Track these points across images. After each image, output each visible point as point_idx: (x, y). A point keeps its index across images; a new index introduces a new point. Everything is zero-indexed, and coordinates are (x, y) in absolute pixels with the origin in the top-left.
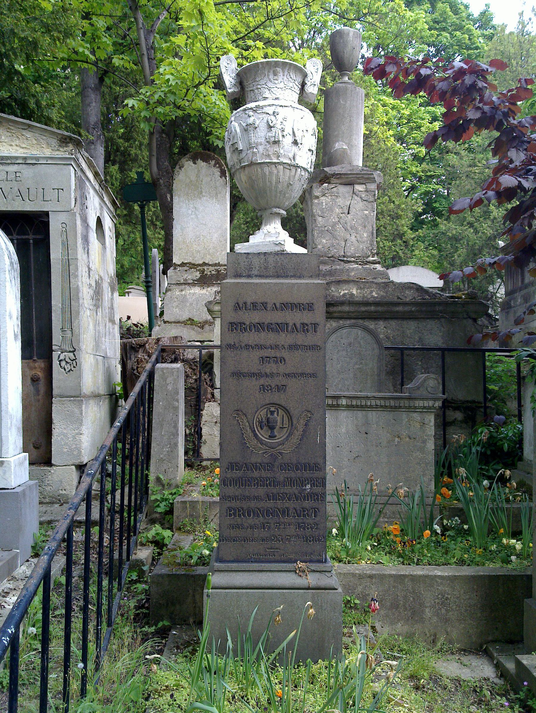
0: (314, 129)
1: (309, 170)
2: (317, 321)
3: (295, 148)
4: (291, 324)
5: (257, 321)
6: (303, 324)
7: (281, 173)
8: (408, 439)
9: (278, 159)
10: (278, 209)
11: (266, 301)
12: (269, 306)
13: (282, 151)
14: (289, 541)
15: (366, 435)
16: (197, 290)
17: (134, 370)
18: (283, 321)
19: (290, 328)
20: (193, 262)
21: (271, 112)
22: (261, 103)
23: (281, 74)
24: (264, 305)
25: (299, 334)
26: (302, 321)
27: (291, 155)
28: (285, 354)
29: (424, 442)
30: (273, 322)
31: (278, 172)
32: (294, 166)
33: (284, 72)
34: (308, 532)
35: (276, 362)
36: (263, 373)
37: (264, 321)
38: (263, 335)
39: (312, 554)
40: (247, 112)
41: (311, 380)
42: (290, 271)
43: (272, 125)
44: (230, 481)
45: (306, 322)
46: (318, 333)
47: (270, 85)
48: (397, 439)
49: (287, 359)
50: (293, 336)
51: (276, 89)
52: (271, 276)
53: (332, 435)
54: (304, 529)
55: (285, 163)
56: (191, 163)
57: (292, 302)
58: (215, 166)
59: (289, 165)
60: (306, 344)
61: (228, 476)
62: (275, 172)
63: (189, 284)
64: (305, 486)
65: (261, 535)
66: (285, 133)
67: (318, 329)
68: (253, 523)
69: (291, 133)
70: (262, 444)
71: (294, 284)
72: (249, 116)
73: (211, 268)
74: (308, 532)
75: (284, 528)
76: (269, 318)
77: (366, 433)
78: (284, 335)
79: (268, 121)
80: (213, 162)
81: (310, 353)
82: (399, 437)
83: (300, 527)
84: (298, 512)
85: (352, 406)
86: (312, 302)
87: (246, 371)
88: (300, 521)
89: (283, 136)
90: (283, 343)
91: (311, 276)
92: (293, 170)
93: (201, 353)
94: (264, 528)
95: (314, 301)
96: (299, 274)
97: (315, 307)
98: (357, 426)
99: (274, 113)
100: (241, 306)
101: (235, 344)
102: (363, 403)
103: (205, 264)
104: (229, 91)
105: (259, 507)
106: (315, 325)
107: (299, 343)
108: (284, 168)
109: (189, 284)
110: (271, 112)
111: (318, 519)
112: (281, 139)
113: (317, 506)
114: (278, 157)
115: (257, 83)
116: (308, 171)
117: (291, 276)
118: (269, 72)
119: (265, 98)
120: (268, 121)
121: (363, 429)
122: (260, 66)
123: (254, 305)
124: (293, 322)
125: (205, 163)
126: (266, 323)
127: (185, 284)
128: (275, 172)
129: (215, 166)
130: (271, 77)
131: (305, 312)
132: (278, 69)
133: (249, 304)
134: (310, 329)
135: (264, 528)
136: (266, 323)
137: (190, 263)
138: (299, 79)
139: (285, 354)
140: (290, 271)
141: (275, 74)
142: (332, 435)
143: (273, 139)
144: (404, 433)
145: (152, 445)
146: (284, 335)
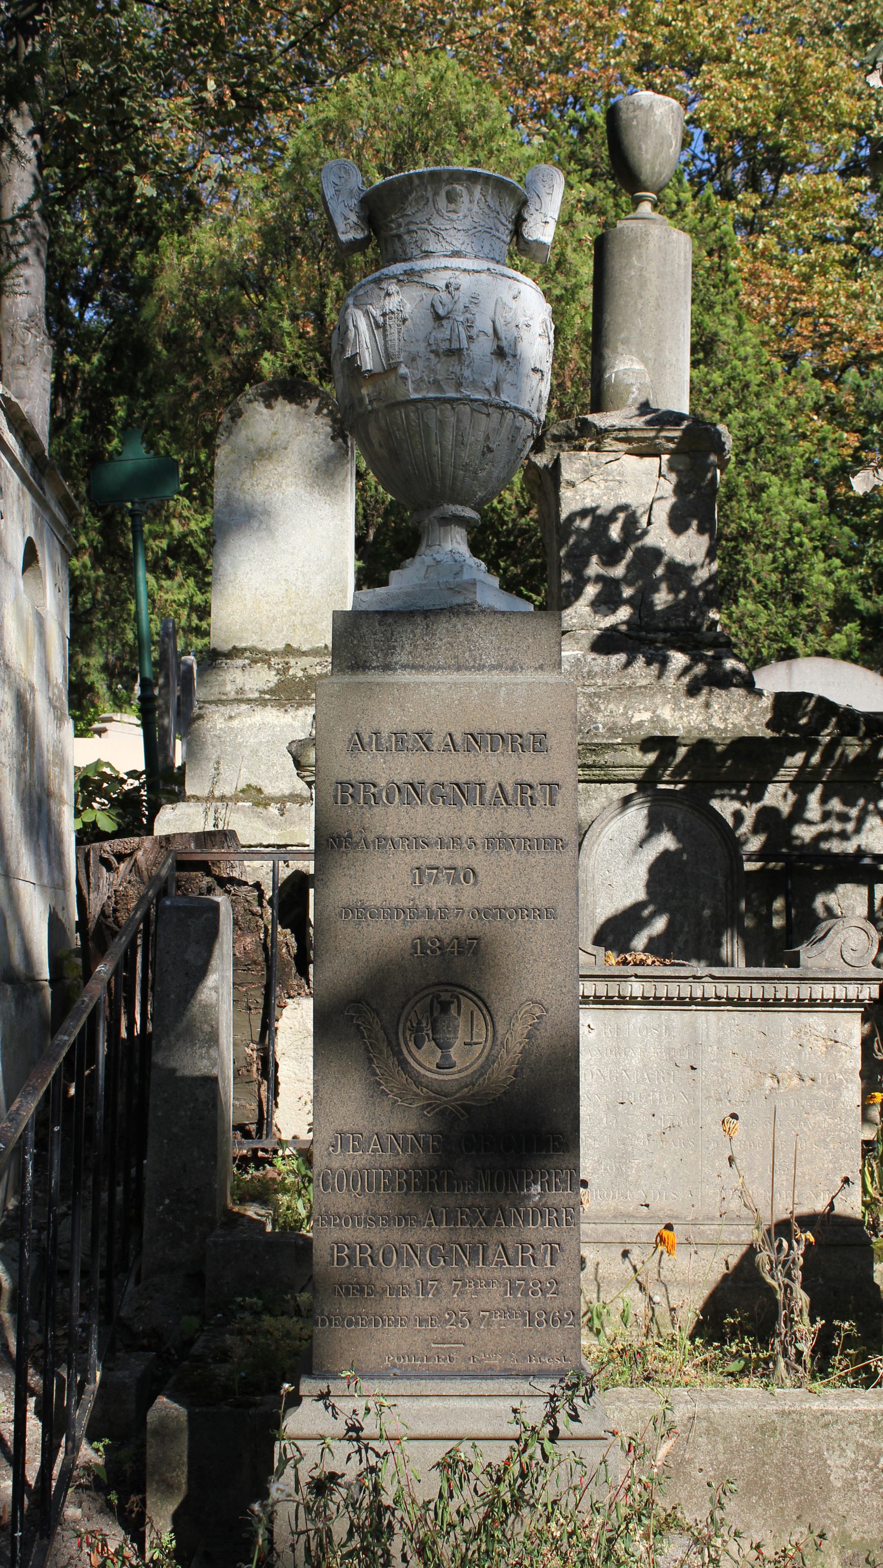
0: (544, 322)
1: (535, 415)
2: (557, 777)
3: (498, 368)
4: (490, 785)
5: (406, 777)
6: (523, 786)
7: (466, 422)
8: (796, 1081)
9: (458, 391)
10: (460, 508)
11: (428, 727)
12: (436, 741)
13: (467, 373)
14: (489, 1324)
15: (692, 1072)
16: (271, 716)
17: (107, 917)
18: (472, 778)
19: (488, 795)
20: (261, 646)
21: (441, 284)
22: (425, 264)
23: (466, 198)
24: (424, 739)
25: (510, 810)
26: (519, 778)
27: (489, 382)
28: (477, 859)
29: (837, 1087)
30: (444, 779)
31: (459, 421)
32: (498, 406)
33: (471, 194)
34: (535, 1302)
35: (455, 880)
36: (421, 907)
37: (423, 777)
38: (421, 811)
39: (544, 1354)
40: (384, 285)
41: (541, 924)
42: (488, 656)
43: (441, 312)
44: (340, 1177)
45: (527, 778)
46: (559, 807)
47: (438, 222)
48: (769, 1082)
49: (481, 873)
50: (498, 814)
51: (452, 232)
52: (440, 668)
53: (606, 1073)
54: (525, 1294)
55: (476, 400)
56: (260, 407)
57: (493, 729)
58: (318, 411)
59: (485, 404)
60: (528, 834)
61: (335, 1165)
62: (452, 420)
63: (249, 701)
64: (528, 1187)
65: (417, 1310)
66: (474, 332)
67: (559, 798)
68: (397, 1281)
69: (490, 331)
70: (418, 1084)
71: (497, 686)
72: (388, 295)
73: (305, 661)
74: (535, 1302)
75: (476, 1293)
76: (437, 769)
77: (693, 1068)
78: (473, 813)
79: (433, 306)
80: (314, 404)
81: (538, 857)
82: (774, 1076)
83: (514, 1289)
84: (510, 1252)
85: (657, 1001)
86: (543, 729)
87: (378, 902)
88: (514, 1274)
89: (470, 338)
90: (470, 832)
91: (541, 667)
92: (496, 415)
93: (275, 870)
94: (425, 1293)
95: (548, 728)
96: (510, 663)
97: (551, 742)
98: (669, 1050)
99: (447, 286)
100: (366, 740)
101: (350, 836)
102: (685, 991)
103: (289, 650)
104: (343, 238)
105: (412, 1240)
106: (553, 786)
107: (512, 832)
108: (473, 410)
109: (249, 701)
110: (441, 284)
111: (558, 1269)
112: (465, 344)
113: (557, 1238)
114: (459, 385)
115: (408, 219)
116: (530, 417)
117: (493, 667)
118: (436, 194)
119: (427, 254)
120: (433, 306)
121: (685, 1060)
122: (416, 182)
123: (400, 738)
124: (497, 779)
125: (294, 407)
126: (428, 782)
127: (240, 701)
128: (452, 420)
129: (318, 411)
130: (442, 202)
131: (527, 756)
132: (458, 188)
133: (385, 735)
134: (538, 794)
135: (425, 1293)
136: (428, 782)
137: (253, 650)
138: (510, 209)
139: (477, 859)
140: (488, 656)
141: (451, 198)
142: (606, 1073)
143: (445, 346)
144: (787, 1066)
145: (152, 1101)
146: (473, 813)
